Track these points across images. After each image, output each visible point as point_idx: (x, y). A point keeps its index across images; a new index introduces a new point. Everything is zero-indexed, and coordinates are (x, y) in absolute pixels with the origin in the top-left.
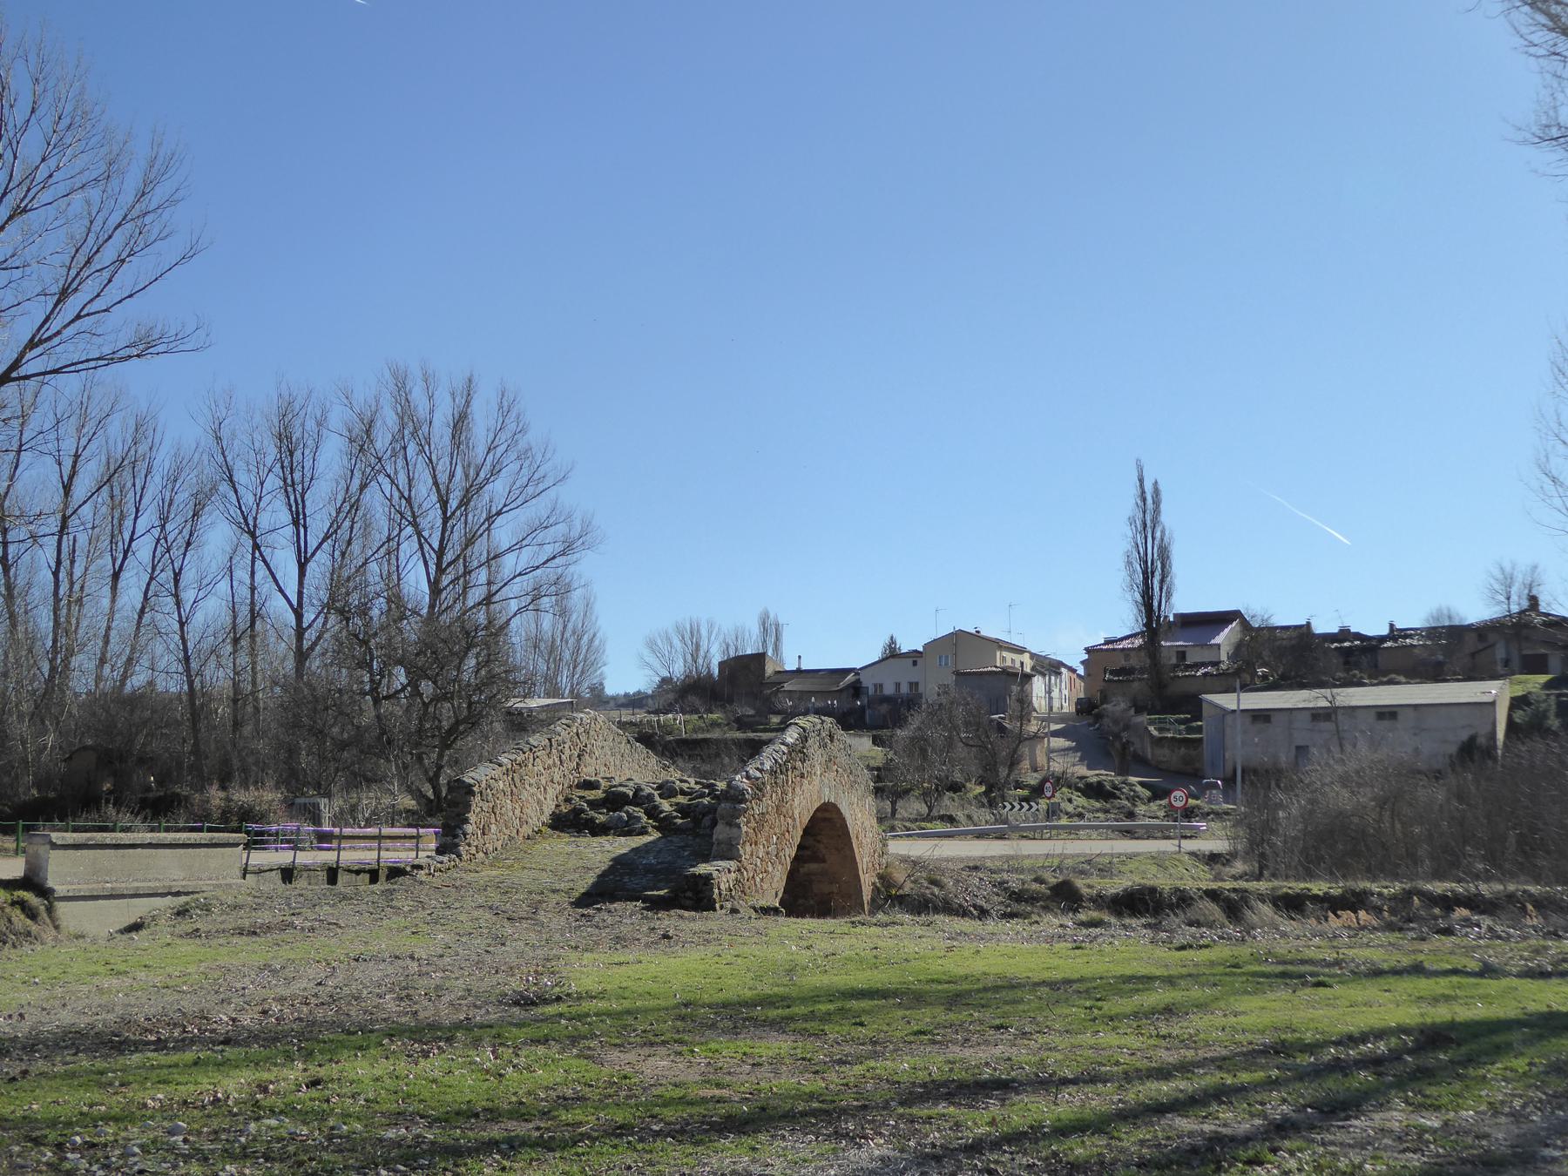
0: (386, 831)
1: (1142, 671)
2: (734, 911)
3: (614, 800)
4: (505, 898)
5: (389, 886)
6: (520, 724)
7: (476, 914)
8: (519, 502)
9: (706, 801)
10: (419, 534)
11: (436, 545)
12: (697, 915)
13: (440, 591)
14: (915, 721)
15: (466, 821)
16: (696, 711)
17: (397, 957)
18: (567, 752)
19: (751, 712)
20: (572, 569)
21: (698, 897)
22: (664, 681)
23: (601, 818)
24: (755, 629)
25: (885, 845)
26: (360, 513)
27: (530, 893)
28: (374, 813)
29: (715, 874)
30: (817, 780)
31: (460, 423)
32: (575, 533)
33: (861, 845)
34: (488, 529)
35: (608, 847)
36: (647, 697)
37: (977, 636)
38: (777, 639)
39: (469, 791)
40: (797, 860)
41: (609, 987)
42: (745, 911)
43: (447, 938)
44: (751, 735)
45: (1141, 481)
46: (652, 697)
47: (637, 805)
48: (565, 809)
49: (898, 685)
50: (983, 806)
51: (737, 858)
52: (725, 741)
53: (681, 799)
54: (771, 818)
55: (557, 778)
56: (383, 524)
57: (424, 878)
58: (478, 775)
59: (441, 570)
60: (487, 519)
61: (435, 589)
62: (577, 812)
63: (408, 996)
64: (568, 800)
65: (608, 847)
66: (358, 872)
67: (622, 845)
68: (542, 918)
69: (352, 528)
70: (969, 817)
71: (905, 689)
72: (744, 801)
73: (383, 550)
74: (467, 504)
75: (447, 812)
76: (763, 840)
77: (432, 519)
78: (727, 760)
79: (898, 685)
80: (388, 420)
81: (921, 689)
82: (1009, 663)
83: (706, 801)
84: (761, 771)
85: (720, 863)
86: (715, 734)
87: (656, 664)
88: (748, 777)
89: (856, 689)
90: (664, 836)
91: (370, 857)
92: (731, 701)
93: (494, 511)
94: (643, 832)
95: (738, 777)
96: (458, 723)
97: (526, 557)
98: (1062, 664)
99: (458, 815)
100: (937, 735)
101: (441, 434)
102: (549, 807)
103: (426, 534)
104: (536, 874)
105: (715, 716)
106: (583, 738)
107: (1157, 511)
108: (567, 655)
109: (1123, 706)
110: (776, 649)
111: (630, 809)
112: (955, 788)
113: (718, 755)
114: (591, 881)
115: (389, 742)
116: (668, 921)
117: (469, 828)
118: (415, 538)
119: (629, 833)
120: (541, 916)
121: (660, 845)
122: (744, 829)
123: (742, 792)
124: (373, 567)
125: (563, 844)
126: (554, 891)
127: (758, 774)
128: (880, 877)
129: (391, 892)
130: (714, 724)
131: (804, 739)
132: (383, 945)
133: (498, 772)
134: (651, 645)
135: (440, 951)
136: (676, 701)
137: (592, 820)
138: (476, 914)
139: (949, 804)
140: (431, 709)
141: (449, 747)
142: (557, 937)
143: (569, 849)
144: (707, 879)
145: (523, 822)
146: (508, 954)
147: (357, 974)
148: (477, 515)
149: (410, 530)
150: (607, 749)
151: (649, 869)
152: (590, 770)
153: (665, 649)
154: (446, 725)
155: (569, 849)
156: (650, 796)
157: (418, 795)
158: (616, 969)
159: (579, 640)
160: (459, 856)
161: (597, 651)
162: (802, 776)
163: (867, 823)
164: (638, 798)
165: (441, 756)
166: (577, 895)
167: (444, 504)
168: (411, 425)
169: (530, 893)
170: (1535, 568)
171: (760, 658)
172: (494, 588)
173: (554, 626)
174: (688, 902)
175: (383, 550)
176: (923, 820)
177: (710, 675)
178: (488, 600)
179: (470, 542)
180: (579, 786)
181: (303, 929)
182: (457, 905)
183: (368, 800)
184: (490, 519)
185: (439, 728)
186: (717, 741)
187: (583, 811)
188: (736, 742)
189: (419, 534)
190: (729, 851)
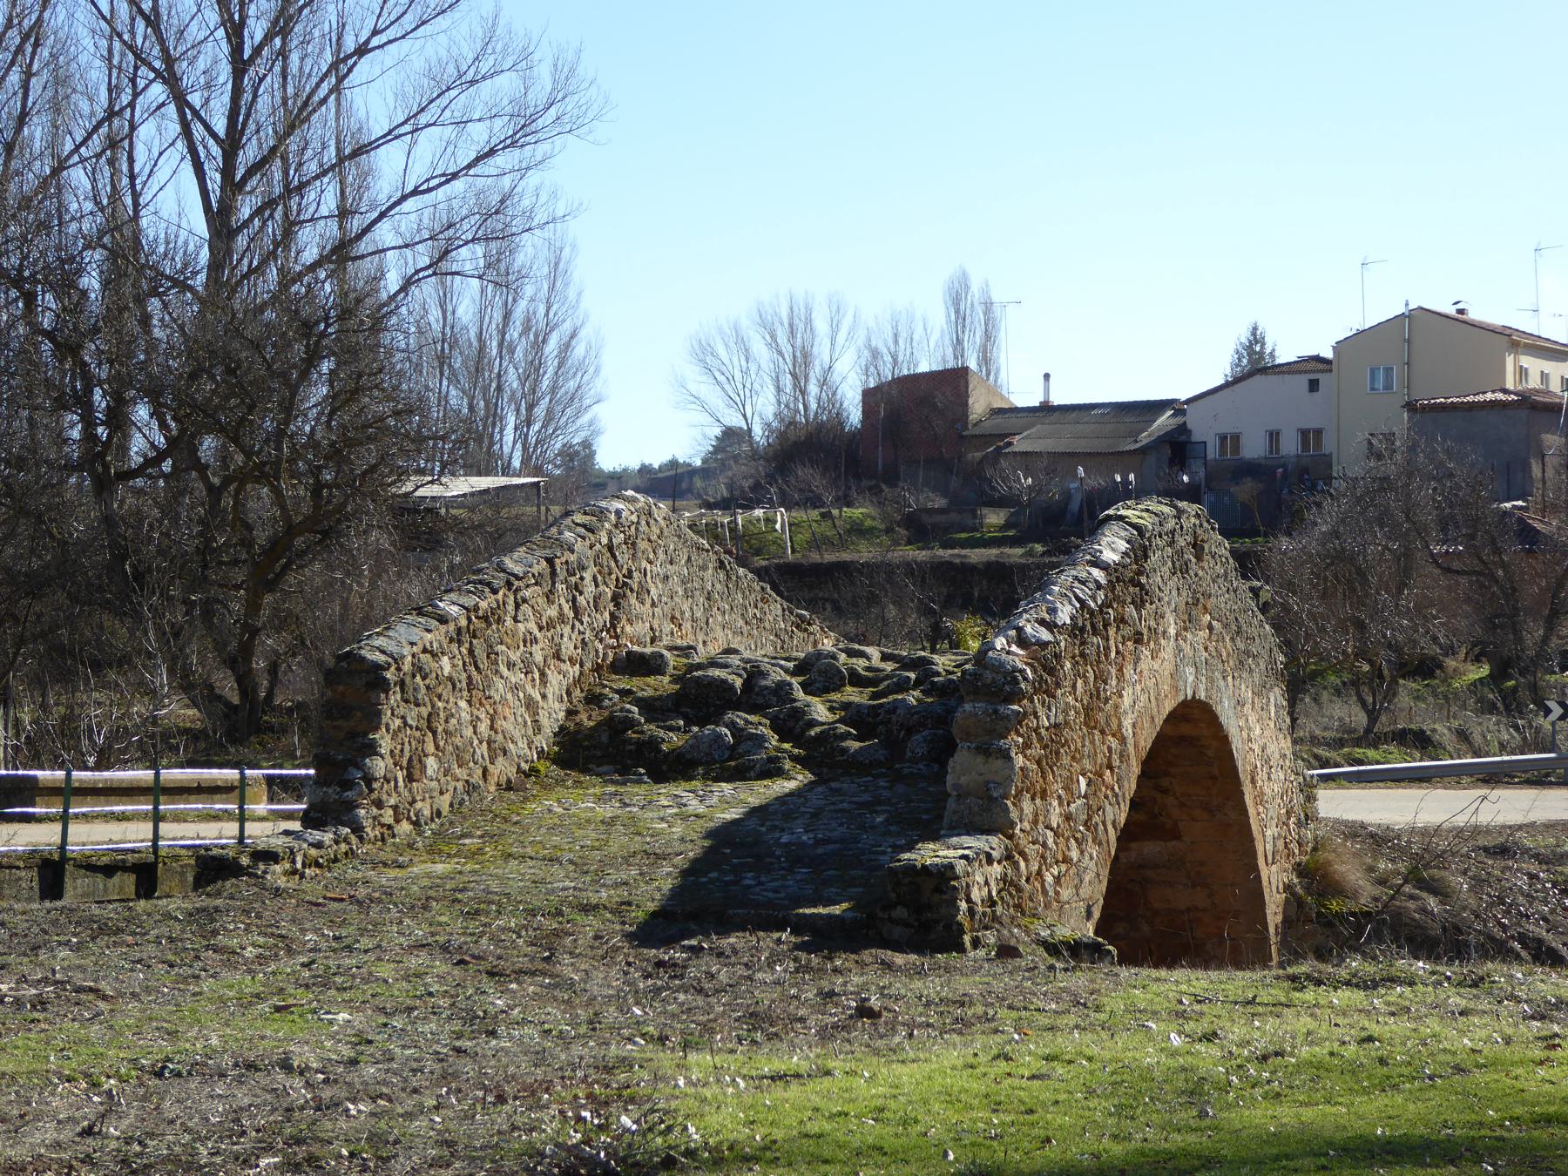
0: (175, 775)
2: (1007, 952)
3: (700, 697)
4: (473, 925)
5: (203, 901)
6: (423, 530)
7: (413, 962)
8: (408, 22)
9: (913, 697)
10: (179, 98)
11: (220, 126)
12: (1163, 973)
13: (233, 234)
14: (1323, 521)
15: (372, 749)
16: (814, 502)
17: (251, 1066)
18: (589, 589)
19: (940, 502)
20: (533, 178)
21: (921, 919)
22: (730, 435)
23: (674, 740)
24: (938, 318)
25: (1311, 798)
27: (532, 913)
28: (114, 736)
29: (960, 866)
30: (1168, 649)
32: (538, 96)
33: (1260, 799)
34: (337, 89)
35: (694, 805)
36: (692, 472)
37: (1459, 320)
38: (988, 336)
39: (374, 679)
40: (1127, 835)
41: (778, 1134)
42: (1034, 956)
43: (359, 1020)
44: (945, 554)
46: (705, 472)
48: (587, 720)
49: (1274, 436)
50: (1491, 708)
51: (1002, 827)
52: (889, 569)
53: (852, 695)
54: (1075, 735)
55: (568, 648)
56: (97, 74)
57: (282, 882)
58: (398, 642)
59: (233, 187)
60: (334, 66)
61: (220, 221)
62: (617, 726)
63: (311, 1159)
64: (593, 699)
65: (694, 805)
66: (109, 870)
67: (728, 802)
68: (568, 972)
69: (26, 87)
70: (1463, 735)
72: (1016, 696)
73: (96, 143)
74: (285, 32)
75: (332, 736)
76: (1058, 788)
77: (208, 63)
78: (892, 612)
79: (1274, 436)
81: (1329, 445)
82: (1534, 382)
83: (913, 697)
84: (1050, 626)
85: (967, 841)
86: (864, 553)
87: (716, 399)
88: (1022, 641)
90: (820, 780)
91: (134, 835)
92: (892, 478)
93: (350, 44)
94: (772, 770)
95: (1000, 642)
96: (291, 530)
97: (428, 152)
99: (352, 735)
100: (1377, 547)
102: (553, 714)
103: (195, 99)
104: (530, 869)
105: (857, 512)
106: (624, 556)
108: (512, 380)
110: (985, 359)
111: (739, 717)
112: (1425, 669)
113: (873, 600)
114: (667, 885)
115: (139, 576)
116: (859, 976)
117: (379, 766)
118: (171, 109)
119: (739, 774)
120: (566, 967)
121: (815, 800)
122: (1019, 761)
123: (1012, 676)
124: (78, 177)
125: (587, 803)
126: (587, 909)
127: (1045, 635)
128: (1301, 870)
129: (211, 914)
130: (858, 530)
131: (1140, 551)
132: (212, 1037)
133: (437, 636)
134: (704, 355)
135: (347, 1052)
136: (771, 479)
137: (654, 743)
138: (413, 962)
139: (1410, 704)
140: (228, 502)
141: (271, 586)
142: (611, 1014)
143: (607, 811)
144: (945, 873)
145: (497, 751)
146: (509, 1049)
147: (170, 1109)
148: (309, 58)
149: (158, 91)
151: (797, 857)
152: (641, 629)
153: (736, 363)
154: (262, 536)
155: (607, 811)
156: (782, 690)
157: (203, 695)
158: (778, 1091)
159: (539, 345)
160: (358, 829)
161: (581, 367)
162: (1138, 639)
163: (1273, 749)
164: (756, 692)
165: (253, 606)
166: (640, 915)
167: (235, 32)
169: (532, 913)
171: (954, 381)
172: (356, 224)
173: (482, 313)
174: (898, 932)
175: (96, 143)
176: (1358, 743)
177: (839, 420)
178: (341, 253)
179: (297, 117)
181: (18, 1003)
182: (366, 942)
183: (97, 708)
184: (341, 67)
185: (247, 544)
186: (869, 568)
187: (630, 723)
188: (910, 568)
189: (179, 98)
190: (986, 814)
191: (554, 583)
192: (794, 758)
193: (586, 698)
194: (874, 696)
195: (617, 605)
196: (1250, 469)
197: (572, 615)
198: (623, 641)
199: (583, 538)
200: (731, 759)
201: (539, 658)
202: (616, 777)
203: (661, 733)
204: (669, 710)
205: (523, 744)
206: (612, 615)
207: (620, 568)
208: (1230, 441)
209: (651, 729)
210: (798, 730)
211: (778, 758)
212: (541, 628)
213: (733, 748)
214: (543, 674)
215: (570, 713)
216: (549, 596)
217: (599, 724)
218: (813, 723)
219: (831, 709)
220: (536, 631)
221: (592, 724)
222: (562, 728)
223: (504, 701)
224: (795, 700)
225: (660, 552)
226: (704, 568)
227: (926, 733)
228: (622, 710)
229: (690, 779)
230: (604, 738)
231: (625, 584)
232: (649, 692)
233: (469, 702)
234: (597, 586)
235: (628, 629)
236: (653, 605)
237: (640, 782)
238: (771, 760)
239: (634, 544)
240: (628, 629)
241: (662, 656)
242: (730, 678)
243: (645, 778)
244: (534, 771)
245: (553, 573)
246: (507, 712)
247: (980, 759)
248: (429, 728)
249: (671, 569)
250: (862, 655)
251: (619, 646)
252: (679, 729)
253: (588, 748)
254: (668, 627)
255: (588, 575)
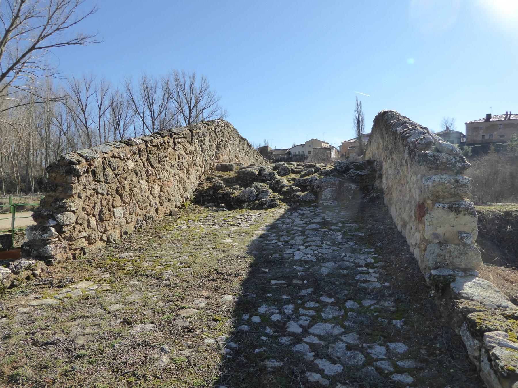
1: (357, 147)
18: (207, 143)
26: (168, 109)
31: (191, 87)
35: (245, 226)
45: (357, 101)
47: (263, 181)
48: (206, 186)
53: (296, 176)
55: (199, 161)
62: (216, 188)
64: (209, 179)
71: (301, 153)
80: (172, 85)
89: (289, 153)
94: (272, 205)
98: (333, 147)
101: (187, 87)
102: (192, 185)
106: (220, 135)
107: (361, 107)
109: (354, 155)
111: (258, 184)
119: (261, 207)
125: (201, 222)
137: (228, 195)
150: (236, 146)
152: (226, 158)
155: (205, 229)
156: (271, 175)
164: (262, 177)
168: (179, 86)
170: (453, 119)
180: (217, 169)
187: (220, 187)
191: (192, 139)
192: (280, 199)
193: (207, 179)
194: (302, 176)
195: (218, 150)
196: (296, 155)
197: (201, 150)
198: (220, 161)
199: (205, 127)
200: (256, 200)
201: (186, 164)
202: (214, 208)
203: (231, 191)
204: (234, 182)
205: (178, 197)
206: (216, 152)
207: (219, 138)
208: (295, 153)
209: (228, 189)
210: (279, 188)
211: (275, 200)
212: (187, 154)
213: (257, 196)
214: (188, 170)
215: (200, 184)
216: (191, 142)
217: (210, 188)
218: (284, 186)
219: (288, 181)
220: (184, 154)
221: (207, 187)
222: (197, 189)
223: (168, 180)
224: (276, 178)
225: (231, 137)
226: (244, 144)
227: (329, 189)
228: (218, 183)
229: (242, 208)
230: (211, 193)
231: (220, 144)
232: (228, 176)
233: (147, 181)
234: (210, 142)
235: (221, 157)
236: (230, 151)
237: (223, 210)
238: (272, 201)
239: (223, 133)
240: (221, 157)
241: (232, 165)
242: (254, 171)
243: (225, 209)
244: (183, 206)
245: (192, 136)
246: (170, 185)
247: (452, 215)
248: (117, 193)
249: (235, 143)
250: (292, 164)
251: (218, 162)
252: (237, 189)
253: (205, 196)
254: (234, 158)
255: (207, 139)
